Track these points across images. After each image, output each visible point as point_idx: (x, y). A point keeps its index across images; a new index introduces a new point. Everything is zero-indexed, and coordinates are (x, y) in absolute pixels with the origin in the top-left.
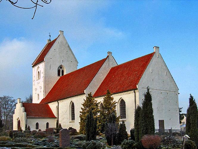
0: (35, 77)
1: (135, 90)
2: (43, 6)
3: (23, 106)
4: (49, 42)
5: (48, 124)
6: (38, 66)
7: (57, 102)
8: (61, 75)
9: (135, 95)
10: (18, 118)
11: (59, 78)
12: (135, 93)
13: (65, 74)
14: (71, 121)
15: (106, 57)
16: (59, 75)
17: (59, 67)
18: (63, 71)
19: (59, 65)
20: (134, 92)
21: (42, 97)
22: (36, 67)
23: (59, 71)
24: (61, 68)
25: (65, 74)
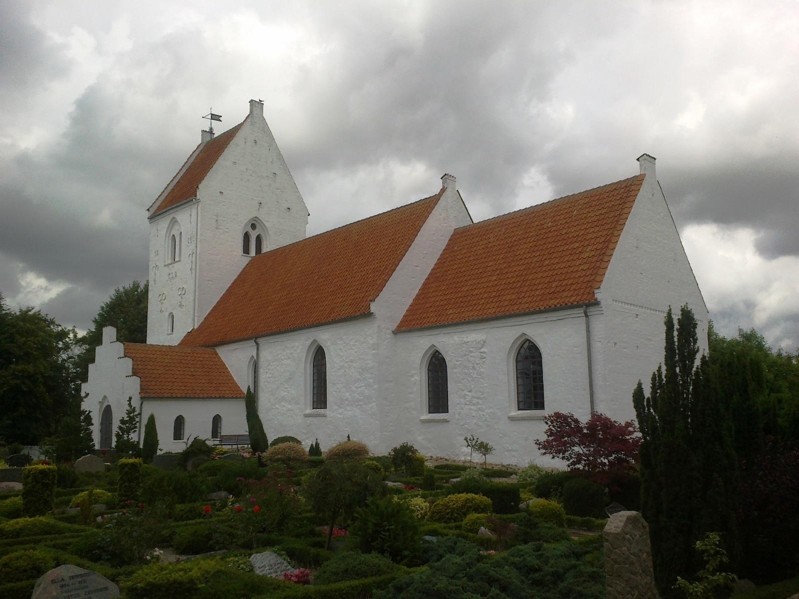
0: (157, 253)
1: (588, 306)
2: (127, 377)
3: (135, 373)
4: (208, 139)
5: (217, 420)
6: (173, 215)
7: (252, 343)
8: (253, 253)
9: (588, 331)
10: (105, 397)
11: (246, 260)
12: (587, 316)
13: (267, 248)
14: (309, 411)
15: (437, 191)
16: (246, 250)
17: (246, 225)
18: (259, 240)
19: (245, 218)
20: (585, 313)
21: (186, 323)
22: (163, 223)
23: (247, 237)
24: (253, 226)
25: (267, 248)
